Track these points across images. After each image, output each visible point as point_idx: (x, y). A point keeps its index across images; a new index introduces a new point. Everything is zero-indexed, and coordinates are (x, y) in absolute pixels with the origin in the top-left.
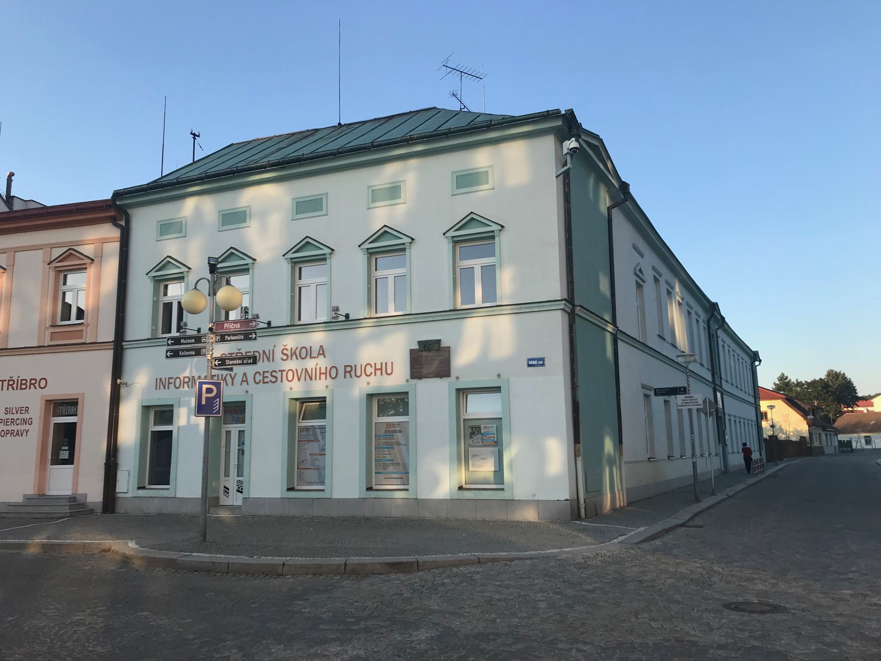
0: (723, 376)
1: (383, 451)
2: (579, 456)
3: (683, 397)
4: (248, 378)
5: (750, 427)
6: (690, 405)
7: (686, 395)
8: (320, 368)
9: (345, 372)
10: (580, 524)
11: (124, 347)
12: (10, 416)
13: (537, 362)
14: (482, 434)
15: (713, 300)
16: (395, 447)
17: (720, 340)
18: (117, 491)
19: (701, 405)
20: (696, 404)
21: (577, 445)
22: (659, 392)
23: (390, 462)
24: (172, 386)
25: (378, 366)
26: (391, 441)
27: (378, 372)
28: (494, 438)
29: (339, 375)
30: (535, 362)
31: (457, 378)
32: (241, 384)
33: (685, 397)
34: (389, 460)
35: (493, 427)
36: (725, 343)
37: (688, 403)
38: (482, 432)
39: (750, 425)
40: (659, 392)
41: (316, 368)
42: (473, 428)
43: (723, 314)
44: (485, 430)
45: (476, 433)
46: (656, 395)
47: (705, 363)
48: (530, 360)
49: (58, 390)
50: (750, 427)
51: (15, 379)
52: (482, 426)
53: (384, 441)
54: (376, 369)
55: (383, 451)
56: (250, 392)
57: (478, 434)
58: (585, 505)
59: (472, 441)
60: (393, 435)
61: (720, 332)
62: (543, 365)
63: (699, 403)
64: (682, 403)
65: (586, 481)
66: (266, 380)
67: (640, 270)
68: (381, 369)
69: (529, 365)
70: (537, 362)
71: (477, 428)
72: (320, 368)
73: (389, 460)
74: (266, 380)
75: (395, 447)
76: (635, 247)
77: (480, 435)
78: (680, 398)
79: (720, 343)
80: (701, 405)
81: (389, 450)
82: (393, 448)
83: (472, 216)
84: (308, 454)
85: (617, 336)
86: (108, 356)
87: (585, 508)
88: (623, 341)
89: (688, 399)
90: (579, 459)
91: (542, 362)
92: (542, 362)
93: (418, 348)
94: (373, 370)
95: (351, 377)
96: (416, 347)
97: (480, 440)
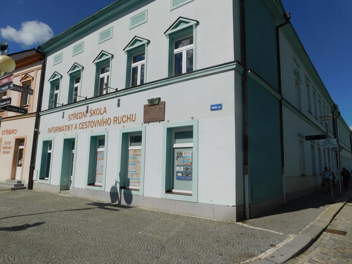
0: (339, 138)
1: (132, 166)
2: (246, 174)
3: (323, 140)
4: (77, 127)
5: (345, 161)
6: (328, 145)
7: (326, 140)
8: (104, 119)
9: (114, 121)
10: (242, 226)
11: (40, 114)
12: (6, 145)
13: (217, 107)
14: (183, 157)
15: (335, 103)
16: (137, 164)
17: (337, 122)
18: (33, 180)
19: (335, 145)
20: (332, 143)
21: (246, 166)
22: (308, 138)
23: (134, 173)
24: (53, 131)
25: (129, 117)
26: (135, 160)
27: (129, 120)
28: (190, 160)
29: (111, 123)
30: (216, 107)
31: (168, 121)
32: (74, 129)
33: (325, 141)
34: (134, 172)
35: (190, 153)
36: (340, 124)
37: (327, 144)
38: (183, 156)
39: (348, 161)
40: (308, 138)
41: (102, 119)
42: (178, 153)
43: (339, 111)
44: (186, 155)
45: (180, 156)
46: (306, 140)
47: (331, 131)
48: (212, 106)
49: (19, 135)
50: (345, 161)
51: (8, 130)
52: (183, 152)
53: (132, 160)
54: (128, 118)
55: (132, 166)
56: (77, 134)
57: (181, 157)
58: (250, 210)
59: (177, 162)
60: (137, 157)
61: (338, 119)
62: (221, 109)
63: (334, 144)
64: (323, 144)
65: (252, 192)
66: (83, 127)
67: (298, 73)
68: (130, 118)
69: (212, 110)
70: (217, 107)
71: (180, 153)
72: (104, 119)
73: (134, 172)
74: (83, 127)
75: (137, 164)
76: (294, 59)
77: (182, 158)
78: (321, 141)
79: (338, 124)
80: (335, 145)
81: (134, 165)
82: (136, 164)
83: (181, 19)
84: (100, 166)
85: (281, 101)
86: (34, 119)
87: (249, 211)
88: (287, 107)
89: (327, 142)
90: (247, 177)
91: (220, 107)
92: (220, 107)
93: (148, 104)
94: (126, 119)
95: (116, 124)
96: (147, 103)
97: (182, 161)
